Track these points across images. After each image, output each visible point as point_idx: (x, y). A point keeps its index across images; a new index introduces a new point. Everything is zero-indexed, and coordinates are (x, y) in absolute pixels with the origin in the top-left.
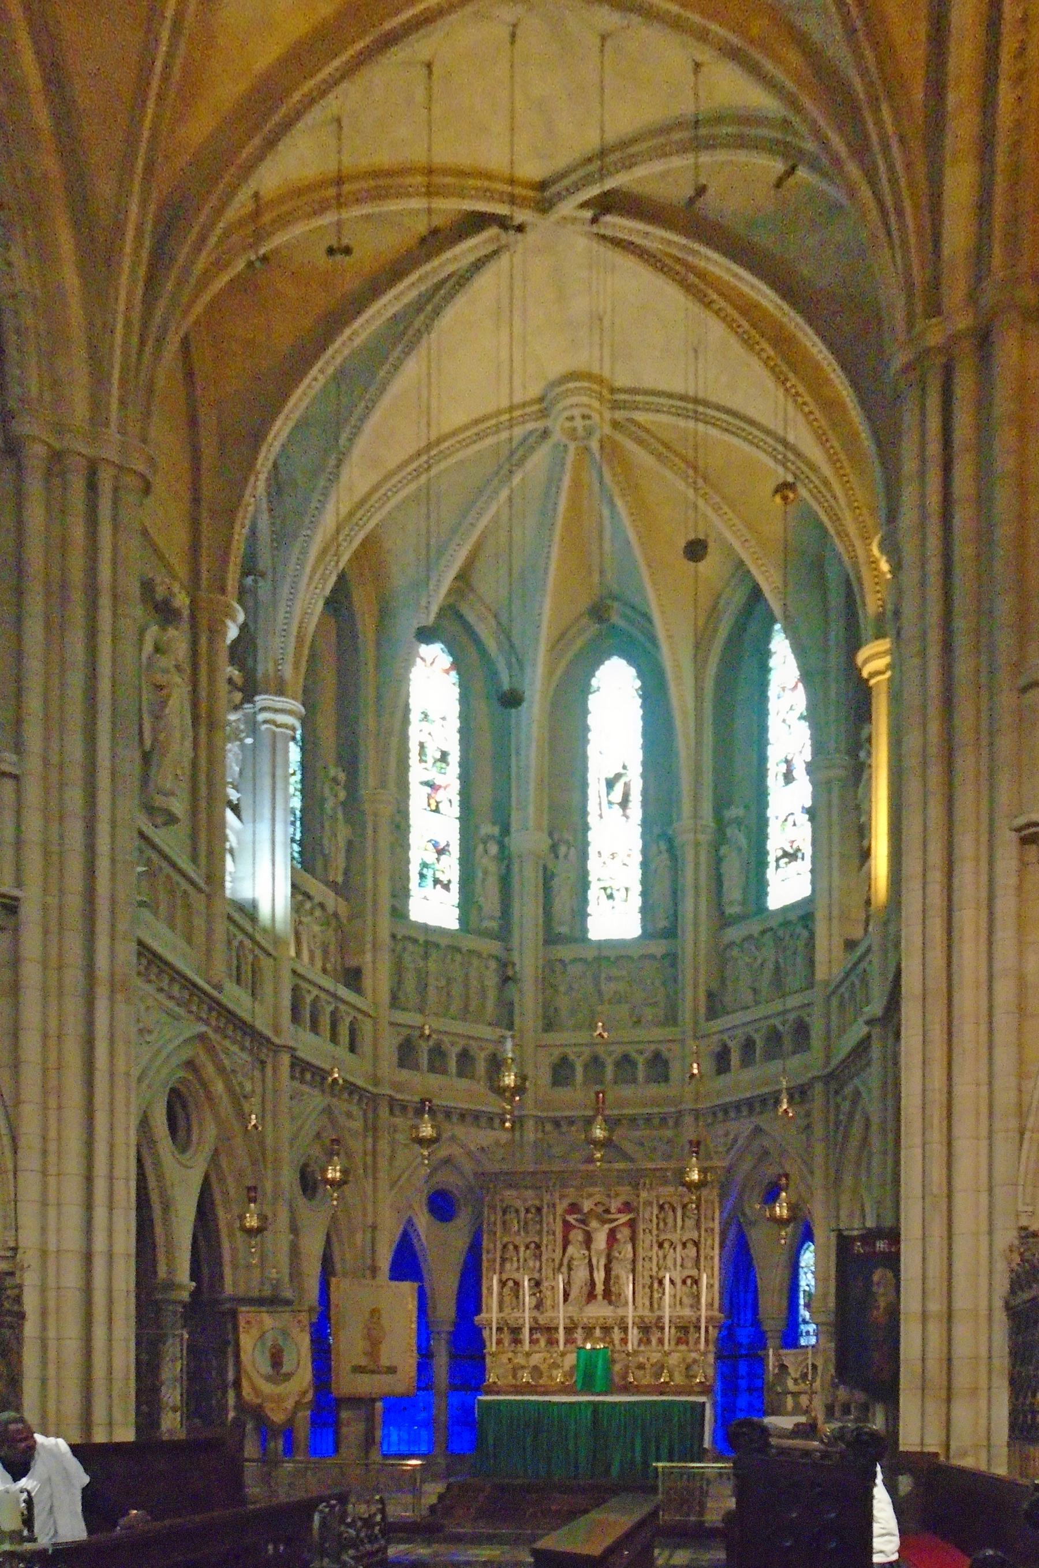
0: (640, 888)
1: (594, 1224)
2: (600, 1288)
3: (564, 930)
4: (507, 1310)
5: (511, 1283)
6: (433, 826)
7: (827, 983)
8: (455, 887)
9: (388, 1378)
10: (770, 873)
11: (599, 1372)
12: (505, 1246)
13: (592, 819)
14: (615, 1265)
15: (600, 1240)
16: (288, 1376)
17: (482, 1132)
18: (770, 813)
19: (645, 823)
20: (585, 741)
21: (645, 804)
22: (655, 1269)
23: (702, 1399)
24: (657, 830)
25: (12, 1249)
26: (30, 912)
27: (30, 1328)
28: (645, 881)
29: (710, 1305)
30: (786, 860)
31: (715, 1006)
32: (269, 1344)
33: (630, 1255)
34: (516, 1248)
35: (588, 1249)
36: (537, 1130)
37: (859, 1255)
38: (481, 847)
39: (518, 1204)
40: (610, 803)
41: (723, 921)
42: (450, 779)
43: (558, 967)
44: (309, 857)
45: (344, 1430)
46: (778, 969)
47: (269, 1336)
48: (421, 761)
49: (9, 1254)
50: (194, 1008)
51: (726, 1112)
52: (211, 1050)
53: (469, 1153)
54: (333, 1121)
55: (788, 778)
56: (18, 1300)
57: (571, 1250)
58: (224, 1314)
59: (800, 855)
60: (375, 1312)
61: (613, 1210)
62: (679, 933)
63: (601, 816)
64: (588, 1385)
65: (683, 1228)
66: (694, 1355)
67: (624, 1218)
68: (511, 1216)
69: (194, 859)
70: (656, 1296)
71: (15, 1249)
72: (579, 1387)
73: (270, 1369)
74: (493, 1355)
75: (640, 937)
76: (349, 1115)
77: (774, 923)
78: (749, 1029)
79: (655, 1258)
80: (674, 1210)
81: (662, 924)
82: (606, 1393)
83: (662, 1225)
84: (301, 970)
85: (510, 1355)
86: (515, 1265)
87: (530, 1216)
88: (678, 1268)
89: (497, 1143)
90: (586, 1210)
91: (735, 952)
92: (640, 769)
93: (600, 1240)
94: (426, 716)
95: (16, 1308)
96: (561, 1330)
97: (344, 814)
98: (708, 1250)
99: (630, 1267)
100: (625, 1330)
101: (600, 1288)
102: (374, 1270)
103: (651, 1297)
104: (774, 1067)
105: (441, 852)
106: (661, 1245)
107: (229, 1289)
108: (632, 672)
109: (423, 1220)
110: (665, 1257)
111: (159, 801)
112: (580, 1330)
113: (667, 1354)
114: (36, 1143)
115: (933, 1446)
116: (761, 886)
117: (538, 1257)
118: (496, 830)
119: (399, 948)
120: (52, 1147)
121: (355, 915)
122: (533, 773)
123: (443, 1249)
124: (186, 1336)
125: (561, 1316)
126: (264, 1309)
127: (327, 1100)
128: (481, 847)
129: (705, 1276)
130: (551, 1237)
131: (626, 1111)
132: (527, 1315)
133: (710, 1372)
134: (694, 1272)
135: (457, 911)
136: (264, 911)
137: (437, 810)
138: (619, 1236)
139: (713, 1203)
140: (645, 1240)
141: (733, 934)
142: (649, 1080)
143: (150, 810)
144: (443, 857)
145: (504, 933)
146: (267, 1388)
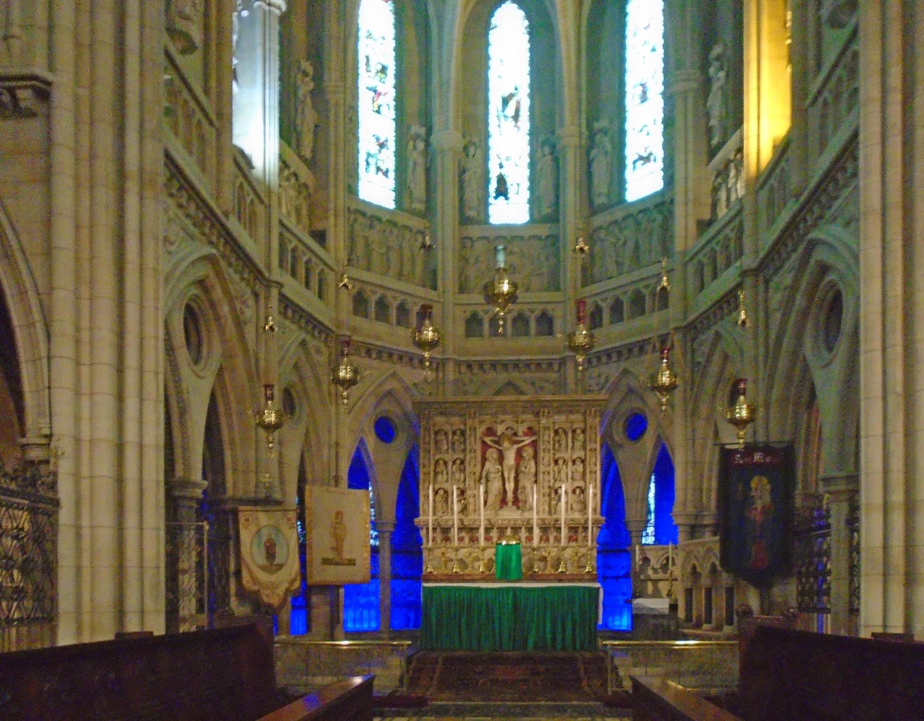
0: (528, 184)
1: (506, 444)
2: (510, 495)
3: (472, 214)
4: (439, 514)
5: (441, 492)
6: (376, 124)
7: (684, 253)
8: (392, 175)
9: (348, 569)
10: (629, 174)
11: (514, 564)
12: (437, 462)
13: (492, 129)
14: (521, 477)
15: (510, 458)
16: (280, 567)
17: (415, 371)
18: (628, 126)
19: (532, 133)
20: (487, 67)
21: (532, 118)
22: (552, 481)
23: (598, 585)
24: (541, 138)
25: (46, 436)
26: (62, 97)
27: (65, 516)
28: (532, 179)
29: (595, 510)
30: (642, 162)
31: (588, 278)
32: (264, 539)
33: (533, 470)
34: (445, 463)
35: (501, 464)
36: (455, 372)
37: (740, 465)
38: (411, 144)
39: (447, 428)
40: (505, 116)
41: (593, 210)
42: (388, 86)
43: (468, 243)
44: (288, 131)
45: (315, 612)
46: (637, 246)
47: (264, 531)
48: (368, 71)
49: (44, 441)
50: (207, 231)
51: (609, 356)
52: (219, 274)
53: (407, 389)
54: (308, 354)
55: (644, 98)
56: (53, 486)
57: (488, 465)
58: (225, 512)
59: (652, 158)
60: (339, 514)
61: (520, 433)
62: (561, 217)
63: (499, 126)
64: (505, 577)
65: (573, 446)
66: (583, 550)
67: (528, 440)
68: (441, 437)
69: (207, 91)
70: (554, 503)
71: (49, 437)
72: (498, 576)
73: (266, 562)
74: (430, 550)
75: (529, 222)
76: (318, 351)
77: (633, 211)
78: (618, 292)
79: (552, 473)
80: (566, 433)
81: (546, 211)
82: (517, 581)
83: (557, 445)
84: (286, 222)
85: (443, 550)
86: (445, 476)
87: (456, 437)
88: (570, 480)
89: (426, 380)
90: (499, 433)
91: (602, 234)
92: (528, 91)
93: (510, 458)
94: (369, 36)
95: (51, 495)
96: (482, 530)
97: (312, 100)
98: (592, 466)
99: (533, 479)
100: (530, 530)
101: (510, 495)
102: (337, 479)
103: (550, 504)
104: (639, 322)
105: (382, 146)
106: (556, 462)
107: (230, 493)
108: (522, 13)
109: (371, 441)
110: (559, 472)
111: (180, 25)
112: (495, 530)
113: (564, 549)
114: (69, 329)
115: (896, 627)
116: (620, 183)
117: (463, 471)
118: (422, 131)
119: (352, 217)
120: (85, 335)
121: (323, 185)
122: (453, 84)
123: (387, 462)
124: (207, 527)
125: (482, 517)
126: (259, 508)
127: (303, 335)
128: (411, 144)
129: (591, 486)
130: (473, 455)
131: (523, 357)
132: (456, 517)
133: (594, 563)
134: (581, 484)
135: (394, 194)
136: (257, 162)
137: (378, 112)
138: (525, 455)
139: (595, 428)
140: (546, 458)
141: (600, 220)
142: (539, 333)
143: (171, 31)
144: (384, 150)
145: (428, 213)
146: (263, 576)
